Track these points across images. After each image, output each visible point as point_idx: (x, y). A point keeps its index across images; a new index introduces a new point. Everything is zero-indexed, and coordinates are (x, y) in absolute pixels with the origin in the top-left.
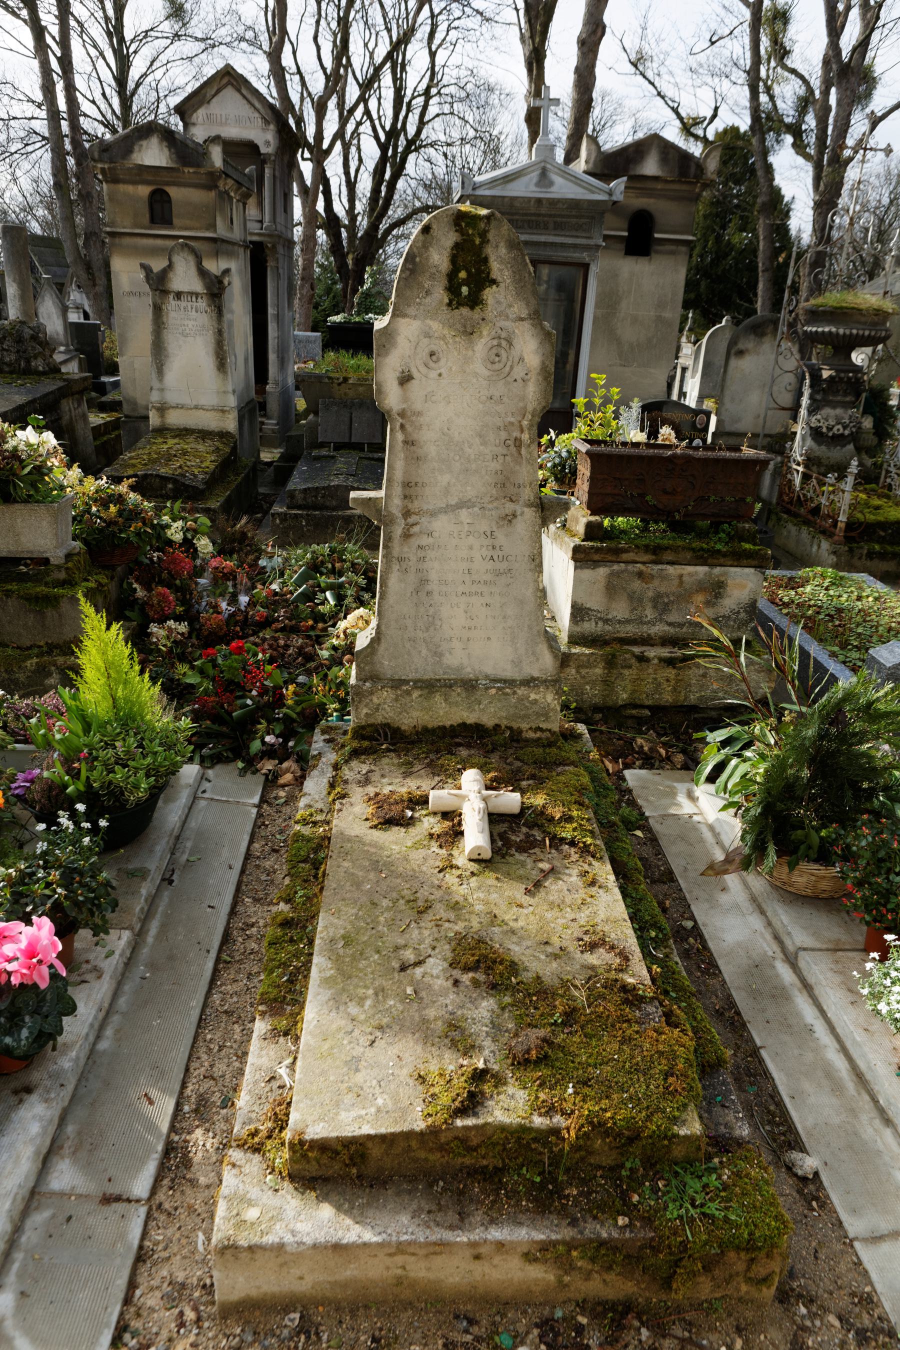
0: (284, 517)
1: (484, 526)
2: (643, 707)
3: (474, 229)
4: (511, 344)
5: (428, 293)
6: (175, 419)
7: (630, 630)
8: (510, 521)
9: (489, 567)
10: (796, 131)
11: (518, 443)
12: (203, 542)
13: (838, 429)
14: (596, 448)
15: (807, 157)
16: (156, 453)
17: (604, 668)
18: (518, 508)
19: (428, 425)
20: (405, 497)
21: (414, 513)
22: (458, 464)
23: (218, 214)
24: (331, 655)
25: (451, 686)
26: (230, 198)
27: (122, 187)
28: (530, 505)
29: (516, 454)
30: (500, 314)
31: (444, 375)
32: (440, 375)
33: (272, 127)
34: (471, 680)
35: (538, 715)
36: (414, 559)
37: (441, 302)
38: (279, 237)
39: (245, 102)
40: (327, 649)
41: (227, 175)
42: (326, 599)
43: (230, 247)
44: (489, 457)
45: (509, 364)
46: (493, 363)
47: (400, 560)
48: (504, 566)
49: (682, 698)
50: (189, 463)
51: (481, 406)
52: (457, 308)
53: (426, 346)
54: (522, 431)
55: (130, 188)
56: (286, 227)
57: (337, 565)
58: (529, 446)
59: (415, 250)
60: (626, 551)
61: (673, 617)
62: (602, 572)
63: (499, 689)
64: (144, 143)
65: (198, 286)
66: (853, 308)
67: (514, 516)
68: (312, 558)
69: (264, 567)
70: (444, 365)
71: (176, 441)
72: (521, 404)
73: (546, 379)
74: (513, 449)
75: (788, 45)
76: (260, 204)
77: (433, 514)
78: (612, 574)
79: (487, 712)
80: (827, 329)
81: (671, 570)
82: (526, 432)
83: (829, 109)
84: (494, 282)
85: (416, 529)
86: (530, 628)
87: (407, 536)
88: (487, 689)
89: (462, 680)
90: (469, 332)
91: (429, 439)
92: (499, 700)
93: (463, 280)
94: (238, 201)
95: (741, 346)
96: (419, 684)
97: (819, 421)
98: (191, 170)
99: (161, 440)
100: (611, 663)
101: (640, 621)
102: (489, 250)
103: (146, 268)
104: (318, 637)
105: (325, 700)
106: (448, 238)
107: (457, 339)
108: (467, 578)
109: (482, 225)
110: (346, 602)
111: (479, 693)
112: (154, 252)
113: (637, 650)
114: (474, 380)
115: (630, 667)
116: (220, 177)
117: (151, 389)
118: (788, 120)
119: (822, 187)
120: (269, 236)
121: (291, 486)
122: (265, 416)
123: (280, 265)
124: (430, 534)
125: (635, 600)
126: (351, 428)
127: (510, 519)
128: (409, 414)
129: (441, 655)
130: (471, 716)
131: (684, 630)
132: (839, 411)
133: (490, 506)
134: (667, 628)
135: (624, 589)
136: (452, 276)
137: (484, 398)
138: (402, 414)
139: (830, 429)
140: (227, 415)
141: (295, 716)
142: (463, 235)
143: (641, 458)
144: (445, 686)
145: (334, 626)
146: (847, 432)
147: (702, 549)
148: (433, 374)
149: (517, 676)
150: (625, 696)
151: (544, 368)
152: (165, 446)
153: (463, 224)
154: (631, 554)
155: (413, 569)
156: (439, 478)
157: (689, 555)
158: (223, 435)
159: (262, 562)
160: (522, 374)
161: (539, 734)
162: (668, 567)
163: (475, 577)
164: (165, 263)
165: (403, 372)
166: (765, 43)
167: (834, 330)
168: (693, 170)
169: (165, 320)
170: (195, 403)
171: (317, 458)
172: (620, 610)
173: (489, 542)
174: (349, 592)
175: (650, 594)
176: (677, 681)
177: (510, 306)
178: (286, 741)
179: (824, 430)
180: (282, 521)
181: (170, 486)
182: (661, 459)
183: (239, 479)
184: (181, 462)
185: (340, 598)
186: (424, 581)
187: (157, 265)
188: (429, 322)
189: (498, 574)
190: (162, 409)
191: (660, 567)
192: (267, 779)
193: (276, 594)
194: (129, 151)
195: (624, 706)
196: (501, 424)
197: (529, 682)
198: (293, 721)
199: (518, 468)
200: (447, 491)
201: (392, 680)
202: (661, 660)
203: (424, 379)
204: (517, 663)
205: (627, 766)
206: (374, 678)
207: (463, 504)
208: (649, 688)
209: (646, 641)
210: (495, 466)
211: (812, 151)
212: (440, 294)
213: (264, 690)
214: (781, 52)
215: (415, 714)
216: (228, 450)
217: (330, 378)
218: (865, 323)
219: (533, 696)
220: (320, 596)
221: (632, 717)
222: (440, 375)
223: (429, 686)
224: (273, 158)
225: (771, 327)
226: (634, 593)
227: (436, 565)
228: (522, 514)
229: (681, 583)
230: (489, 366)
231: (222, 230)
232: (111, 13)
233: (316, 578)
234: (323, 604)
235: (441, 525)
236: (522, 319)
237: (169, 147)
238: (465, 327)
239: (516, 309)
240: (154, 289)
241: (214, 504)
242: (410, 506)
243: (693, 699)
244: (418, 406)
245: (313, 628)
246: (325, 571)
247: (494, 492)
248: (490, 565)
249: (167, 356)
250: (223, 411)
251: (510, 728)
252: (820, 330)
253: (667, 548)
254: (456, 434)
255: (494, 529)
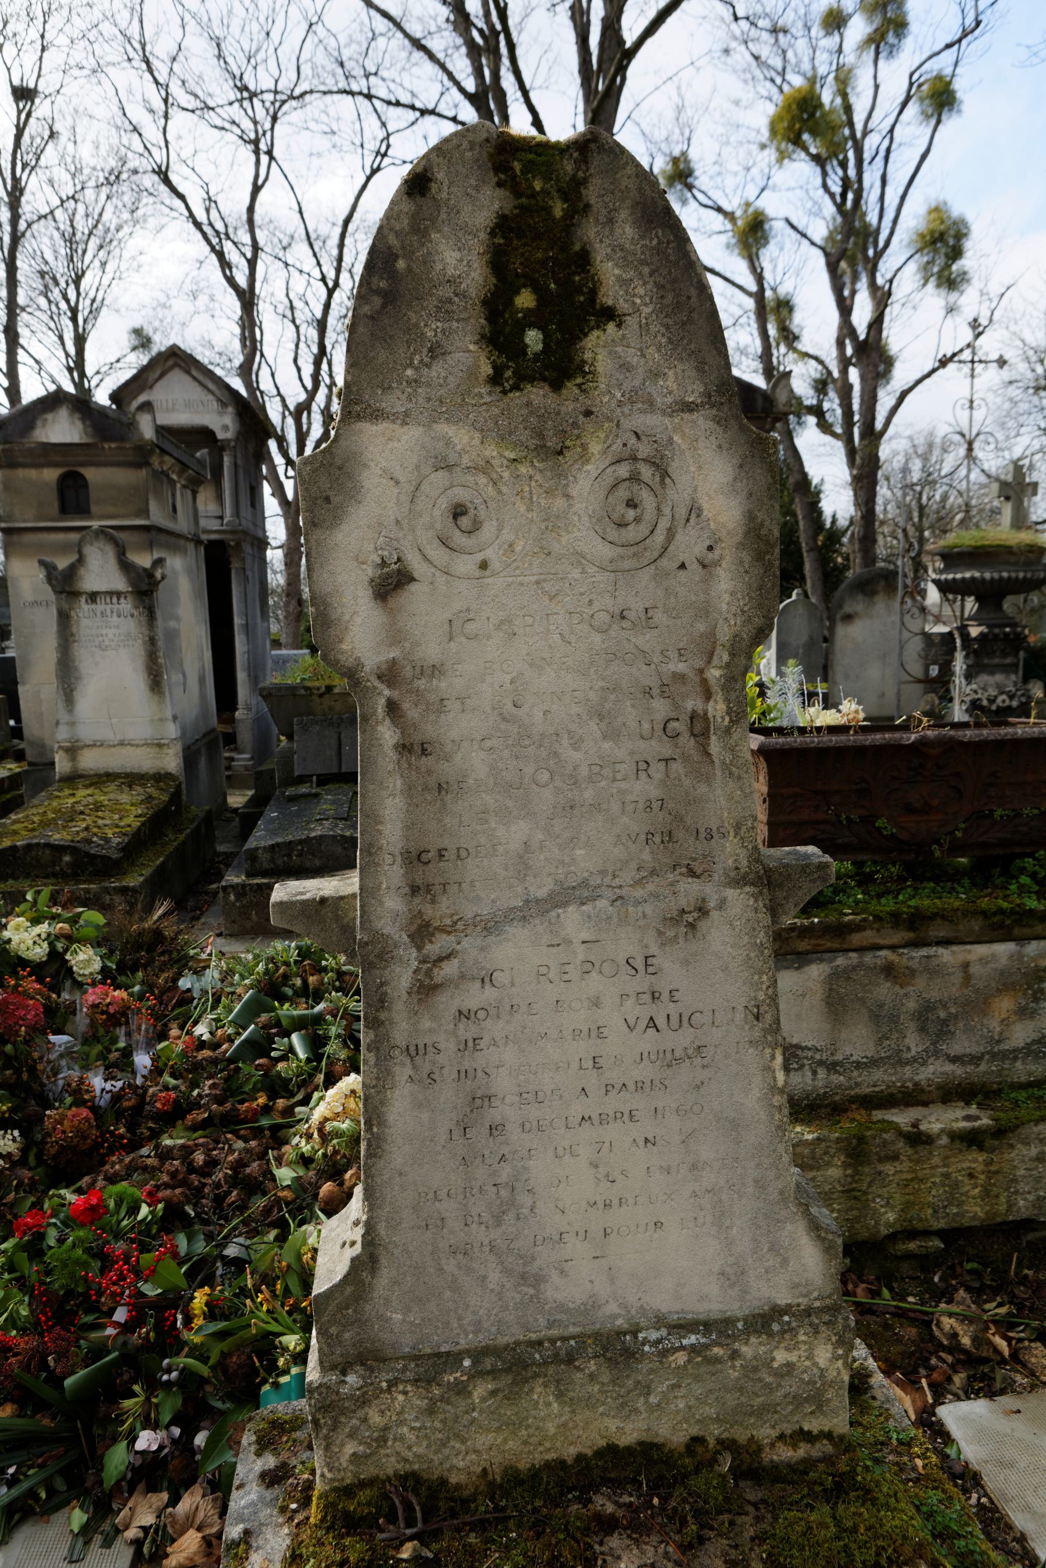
0: (241, 890)
1: (626, 944)
2: (927, 1233)
3: (547, 179)
4: (665, 474)
5: (435, 352)
6: (90, 761)
7: (879, 1079)
8: (692, 926)
9: (646, 1047)
10: (818, 411)
11: (700, 726)
12: (82, 956)
13: (1002, 700)
14: (777, 741)
15: (834, 435)
16: (54, 811)
17: (845, 1165)
18: (710, 891)
19: (461, 699)
20: (415, 890)
21: (442, 930)
22: (547, 794)
23: (151, 497)
24: (297, 1179)
25: (570, 1360)
26: (172, 483)
27: (21, 473)
28: (739, 881)
29: (696, 756)
30: (632, 397)
31: (495, 565)
32: (484, 565)
33: (230, 409)
34: (620, 1333)
35: (798, 1401)
36: (448, 1046)
37: (472, 373)
38: (245, 533)
39: (196, 384)
40: (289, 1164)
41: (163, 451)
42: (291, 1049)
43: (173, 540)
44: (627, 768)
45: (664, 524)
46: (621, 525)
47: (413, 1052)
48: (684, 1039)
49: (1003, 1208)
50: (100, 822)
51: (597, 638)
52: (516, 387)
53: (439, 492)
54: (708, 695)
55: (33, 473)
56: (255, 524)
57: (312, 980)
58: (728, 731)
59: (392, 240)
60: (857, 928)
61: (961, 1045)
62: (816, 972)
63: (693, 1349)
64: (49, 417)
65: (120, 583)
66: (998, 546)
67: (703, 911)
68: (267, 971)
69: (189, 990)
70: (491, 541)
71: (89, 791)
72: (701, 627)
73: (759, 557)
74: (687, 743)
75: (796, 331)
76: (220, 498)
77: (491, 926)
78: (835, 976)
79: (667, 1413)
80: (968, 575)
81: (946, 955)
82: (719, 697)
83: (851, 387)
84: (609, 314)
85: (449, 969)
86: (760, 1185)
87: (426, 989)
88: (664, 1353)
89: (597, 1336)
90: (553, 449)
91: (467, 736)
92: (697, 1378)
93: (528, 312)
94: (184, 486)
95: (847, 609)
96: (488, 1363)
97: (976, 692)
98: (113, 445)
99: (67, 792)
100: (857, 1152)
101: (898, 1060)
102: (590, 232)
103: (49, 569)
104: (275, 1128)
105: (274, 1327)
106: (482, 206)
107: (523, 469)
108: (592, 1081)
109: (569, 167)
110: (328, 1049)
111: (644, 1366)
112: (63, 549)
113: (902, 1118)
114: (575, 574)
115: (895, 1157)
116: (151, 452)
117: (57, 723)
118: (807, 402)
119: (858, 461)
120: (232, 532)
121: (252, 843)
122: (236, 750)
123: (248, 566)
124: (487, 979)
125: (884, 1020)
126: (339, 754)
127: (691, 919)
128: (408, 672)
129: (538, 1280)
130: (629, 1427)
131: (983, 1067)
132: (999, 677)
133: (639, 893)
134: (949, 1068)
135: (862, 1001)
136: (496, 302)
137: (604, 617)
138: (390, 675)
139: (992, 701)
140: (165, 750)
141: (205, 1371)
142: (517, 194)
143: (861, 750)
144: (556, 1359)
145: (305, 1101)
146: (1015, 703)
147: (1001, 911)
148: (466, 565)
149: (735, 1308)
150: (891, 1217)
151: (753, 531)
152: (71, 800)
153: (517, 166)
154: (868, 933)
155: (449, 1074)
156: (501, 832)
157: (976, 925)
158: (160, 778)
159: (184, 983)
160: (699, 549)
161: (802, 1451)
162: (941, 950)
163: (614, 1076)
164: (73, 558)
165: (384, 563)
166: (772, 331)
167: (977, 574)
168: (760, 403)
169: (74, 630)
170: (119, 737)
171: (293, 799)
172: (858, 1042)
173: (642, 983)
174: (333, 1030)
175: (911, 1005)
176: (990, 1175)
177: (656, 375)
178: (189, 1433)
179: (985, 703)
180: (238, 897)
181: (67, 858)
182: (898, 748)
183: (182, 837)
184: (89, 820)
185: (316, 1044)
186: (480, 1101)
187: (62, 563)
188: (443, 428)
189: (671, 1061)
190: (73, 750)
191: (924, 952)
192: (138, 1556)
193: (201, 1045)
194: (30, 426)
195: (893, 1237)
196: (654, 682)
197: (766, 1321)
198: (203, 1381)
199: (702, 789)
200: (523, 864)
201: (416, 1358)
202: (956, 1137)
203: (441, 579)
204: (733, 1277)
205: (940, 1392)
206: (368, 1357)
207: (563, 897)
208: (936, 1195)
209: (911, 1097)
210: (644, 788)
211: (839, 430)
212: (467, 354)
213: (140, 1307)
214: (789, 337)
215: (483, 1440)
216: (165, 798)
217: (307, 688)
218: (1016, 564)
219: (781, 1357)
220: (281, 1043)
221: (909, 1256)
222: (484, 565)
223: (514, 1365)
224: (233, 444)
225: (882, 583)
226: (881, 1006)
227: (509, 1055)
228: (722, 904)
229: (967, 978)
230: (613, 533)
231: (157, 515)
232: (72, 351)
233: (273, 1009)
234: (284, 1058)
235: (516, 952)
236: (689, 408)
237: (83, 420)
238: (541, 436)
239: (671, 383)
240: (58, 592)
241: (134, 880)
242: (429, 911)
243: (1023, 1207)
244: (431, 651)
245: (266, 1110)
246: (289, 992)
247: (646, 855)
248: (649, 1041)
249: (78, 678)
250: (160, 746)
251: (728, 1445)
252: (959, 576)
253: (934, 916)
254: (538, 715)
255: (654, 949)
